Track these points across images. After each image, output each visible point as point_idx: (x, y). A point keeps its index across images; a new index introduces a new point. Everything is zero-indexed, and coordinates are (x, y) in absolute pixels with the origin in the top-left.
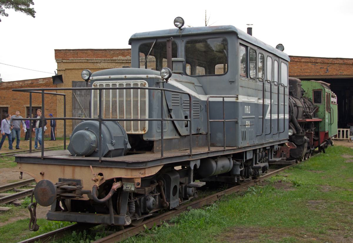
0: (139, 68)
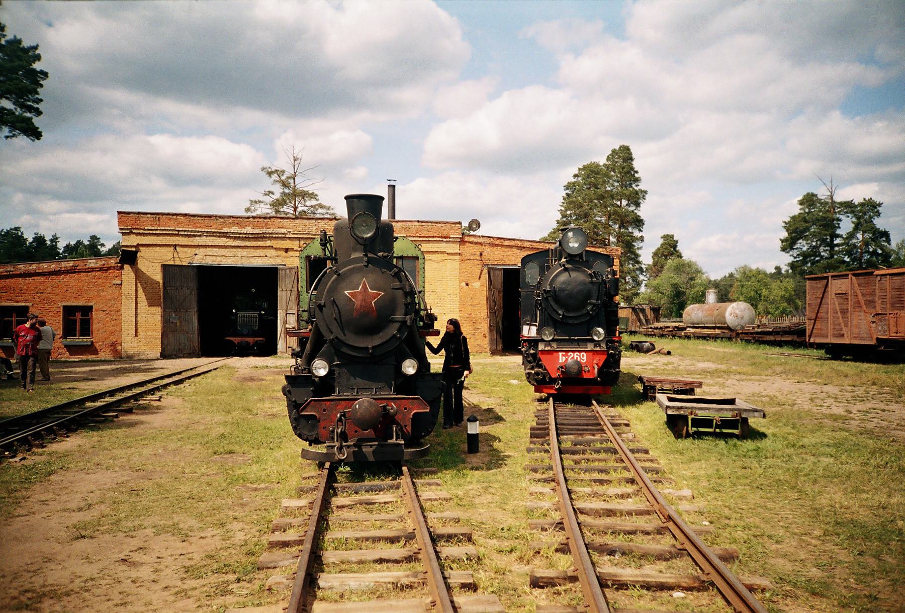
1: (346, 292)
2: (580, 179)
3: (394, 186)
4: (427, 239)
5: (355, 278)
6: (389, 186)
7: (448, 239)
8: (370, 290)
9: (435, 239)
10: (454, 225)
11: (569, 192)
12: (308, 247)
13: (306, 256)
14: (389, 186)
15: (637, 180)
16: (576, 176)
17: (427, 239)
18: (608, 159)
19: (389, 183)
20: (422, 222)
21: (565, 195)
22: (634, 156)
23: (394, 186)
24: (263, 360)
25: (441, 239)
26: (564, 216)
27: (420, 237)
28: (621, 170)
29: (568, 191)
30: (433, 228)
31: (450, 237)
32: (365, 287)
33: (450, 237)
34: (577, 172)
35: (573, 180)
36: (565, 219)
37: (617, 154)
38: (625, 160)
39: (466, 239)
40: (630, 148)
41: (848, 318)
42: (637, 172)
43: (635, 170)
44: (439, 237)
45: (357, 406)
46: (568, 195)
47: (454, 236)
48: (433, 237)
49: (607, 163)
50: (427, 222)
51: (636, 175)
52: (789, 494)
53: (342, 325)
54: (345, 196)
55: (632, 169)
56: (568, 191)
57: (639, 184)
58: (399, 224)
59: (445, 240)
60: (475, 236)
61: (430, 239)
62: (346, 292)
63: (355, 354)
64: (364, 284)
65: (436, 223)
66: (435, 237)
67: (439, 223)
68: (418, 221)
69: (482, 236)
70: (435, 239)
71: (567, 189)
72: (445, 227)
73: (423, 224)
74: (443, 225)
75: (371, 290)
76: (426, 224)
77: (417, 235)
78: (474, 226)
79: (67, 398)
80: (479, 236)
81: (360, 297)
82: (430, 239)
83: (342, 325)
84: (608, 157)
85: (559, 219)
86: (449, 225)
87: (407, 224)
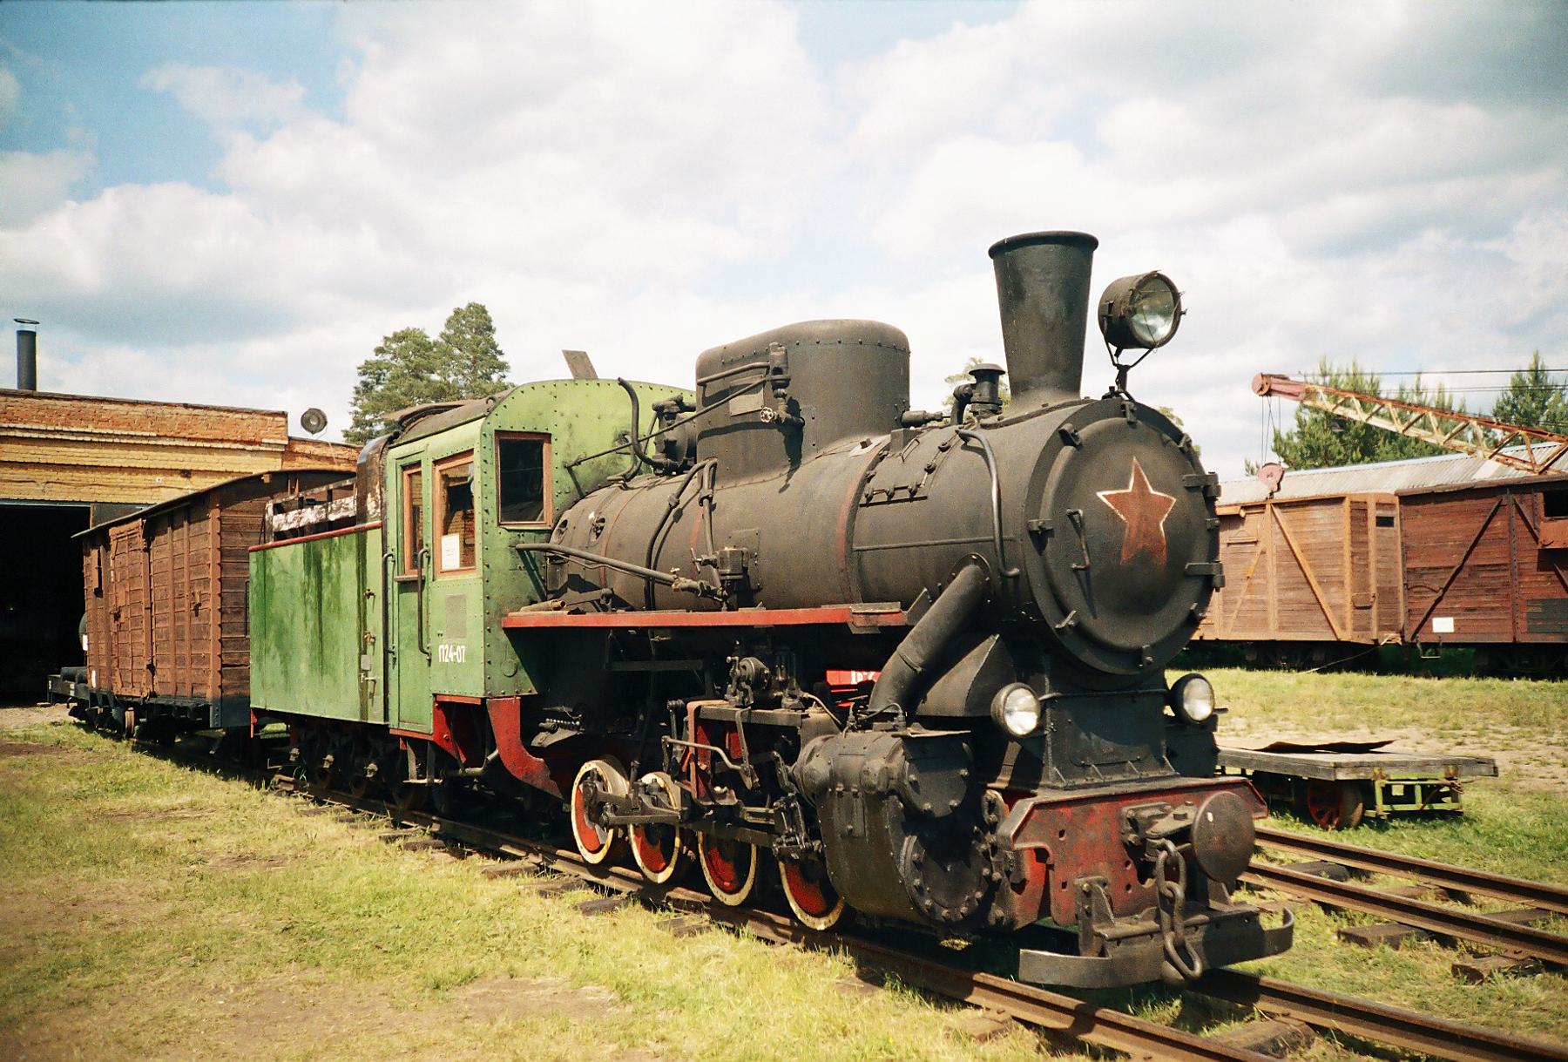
0: (472, 450)
1: (1100, 495)
2: (388, 357)
3: (33, 334)
4: (207, 445)
5: (1115, 456)
6: (21, 333)
7: (257, 447)
8: (1152, 491)
9: (227, 445)
10: (270, 418)
11: (370, 380)
12: (500, 409)
13: (497, 432)
14: (21, 333)
15: (502, 367)
16: (379, 351)
17: (207, 445)
18: (449, 323)
19: (19, 326)
20: (195, 407)
21: (358, 385)
22: (494, 325)
23: (33, 334)
24: (1254, 685)
25: (241, 447)
26: (358, 423)
27: (190, 439)
28: (475, 347)
29: (364, 378)
30: (221, 421)
31: (260, 443)
32: (1140, 483)
33: (260, 443)
34: (381, 344)
35: (373, 358)
36: (358, 430)
37: (464, 318)
38: (479, 331)
39: (298, 448)
40: (487, 309)
41: (1378, 569)
42: (501, 353)
43: (498, 349)
44: (235, 442)
45: (1210, 817)
46: (365, 384)
47: (271, 441)
48: (222, 441)
49: (448, 332)
50: (206, 408)
51: (500, 359)
52: (87, 985)
53: (1088, 584)
54: (588, 353)
55: (494, 347)
56: (364, 378)
57: (506, 374)
58: (138, 408)
59: (249, 448)
60: (316, 443)
61: (214, 445)
62: (1100, 495)
63: (1106, 667)
64: (1138, 473)
65: (229, 411)
66: (228, 441)
67: (236, 411)
68: (186, 406)
69: (333, 444)
70: (227, 445)
71: (364, 373)
72: (250, 422)
73: (196, 411)
74: (245, 416)
75: (1154, 488)
76: (205, 412)
77: (182, 434)
78: (314, 423)
79: (1264, 898)
80: (327, 444)
81: (1135, 508)
82: (214, 445)
83: (1088, 584)
84: (449, 321)
85: (348, 429)
86: (259, 417)
87: (158, 410)
